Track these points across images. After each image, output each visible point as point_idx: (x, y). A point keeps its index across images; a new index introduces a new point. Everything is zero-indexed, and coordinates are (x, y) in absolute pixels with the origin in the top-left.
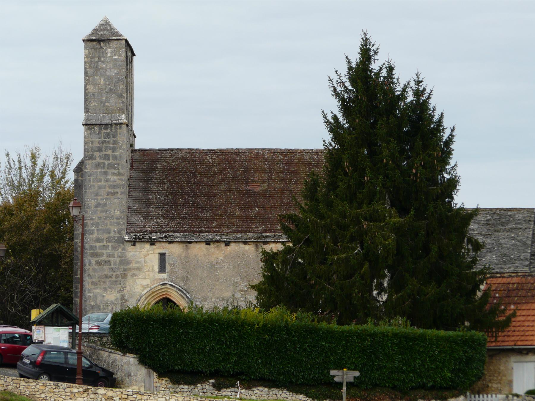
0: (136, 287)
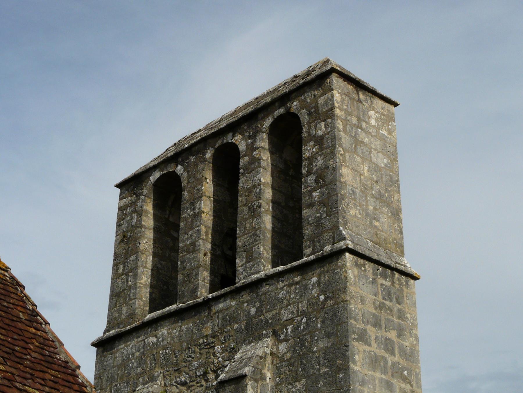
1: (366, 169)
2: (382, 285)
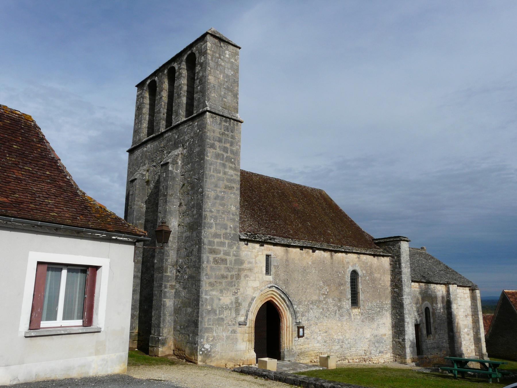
0: (248, 290)
1: (222, 76)
2: (224, 125)
